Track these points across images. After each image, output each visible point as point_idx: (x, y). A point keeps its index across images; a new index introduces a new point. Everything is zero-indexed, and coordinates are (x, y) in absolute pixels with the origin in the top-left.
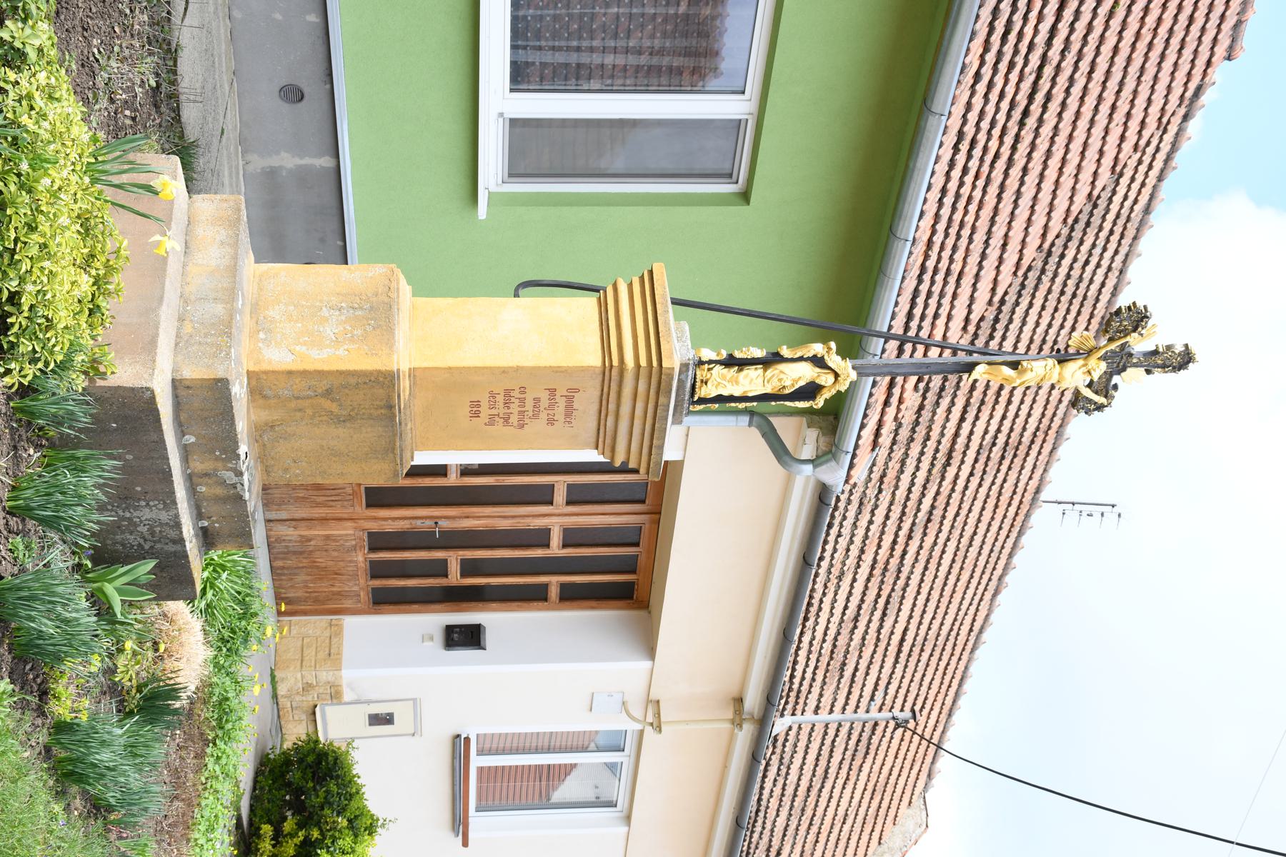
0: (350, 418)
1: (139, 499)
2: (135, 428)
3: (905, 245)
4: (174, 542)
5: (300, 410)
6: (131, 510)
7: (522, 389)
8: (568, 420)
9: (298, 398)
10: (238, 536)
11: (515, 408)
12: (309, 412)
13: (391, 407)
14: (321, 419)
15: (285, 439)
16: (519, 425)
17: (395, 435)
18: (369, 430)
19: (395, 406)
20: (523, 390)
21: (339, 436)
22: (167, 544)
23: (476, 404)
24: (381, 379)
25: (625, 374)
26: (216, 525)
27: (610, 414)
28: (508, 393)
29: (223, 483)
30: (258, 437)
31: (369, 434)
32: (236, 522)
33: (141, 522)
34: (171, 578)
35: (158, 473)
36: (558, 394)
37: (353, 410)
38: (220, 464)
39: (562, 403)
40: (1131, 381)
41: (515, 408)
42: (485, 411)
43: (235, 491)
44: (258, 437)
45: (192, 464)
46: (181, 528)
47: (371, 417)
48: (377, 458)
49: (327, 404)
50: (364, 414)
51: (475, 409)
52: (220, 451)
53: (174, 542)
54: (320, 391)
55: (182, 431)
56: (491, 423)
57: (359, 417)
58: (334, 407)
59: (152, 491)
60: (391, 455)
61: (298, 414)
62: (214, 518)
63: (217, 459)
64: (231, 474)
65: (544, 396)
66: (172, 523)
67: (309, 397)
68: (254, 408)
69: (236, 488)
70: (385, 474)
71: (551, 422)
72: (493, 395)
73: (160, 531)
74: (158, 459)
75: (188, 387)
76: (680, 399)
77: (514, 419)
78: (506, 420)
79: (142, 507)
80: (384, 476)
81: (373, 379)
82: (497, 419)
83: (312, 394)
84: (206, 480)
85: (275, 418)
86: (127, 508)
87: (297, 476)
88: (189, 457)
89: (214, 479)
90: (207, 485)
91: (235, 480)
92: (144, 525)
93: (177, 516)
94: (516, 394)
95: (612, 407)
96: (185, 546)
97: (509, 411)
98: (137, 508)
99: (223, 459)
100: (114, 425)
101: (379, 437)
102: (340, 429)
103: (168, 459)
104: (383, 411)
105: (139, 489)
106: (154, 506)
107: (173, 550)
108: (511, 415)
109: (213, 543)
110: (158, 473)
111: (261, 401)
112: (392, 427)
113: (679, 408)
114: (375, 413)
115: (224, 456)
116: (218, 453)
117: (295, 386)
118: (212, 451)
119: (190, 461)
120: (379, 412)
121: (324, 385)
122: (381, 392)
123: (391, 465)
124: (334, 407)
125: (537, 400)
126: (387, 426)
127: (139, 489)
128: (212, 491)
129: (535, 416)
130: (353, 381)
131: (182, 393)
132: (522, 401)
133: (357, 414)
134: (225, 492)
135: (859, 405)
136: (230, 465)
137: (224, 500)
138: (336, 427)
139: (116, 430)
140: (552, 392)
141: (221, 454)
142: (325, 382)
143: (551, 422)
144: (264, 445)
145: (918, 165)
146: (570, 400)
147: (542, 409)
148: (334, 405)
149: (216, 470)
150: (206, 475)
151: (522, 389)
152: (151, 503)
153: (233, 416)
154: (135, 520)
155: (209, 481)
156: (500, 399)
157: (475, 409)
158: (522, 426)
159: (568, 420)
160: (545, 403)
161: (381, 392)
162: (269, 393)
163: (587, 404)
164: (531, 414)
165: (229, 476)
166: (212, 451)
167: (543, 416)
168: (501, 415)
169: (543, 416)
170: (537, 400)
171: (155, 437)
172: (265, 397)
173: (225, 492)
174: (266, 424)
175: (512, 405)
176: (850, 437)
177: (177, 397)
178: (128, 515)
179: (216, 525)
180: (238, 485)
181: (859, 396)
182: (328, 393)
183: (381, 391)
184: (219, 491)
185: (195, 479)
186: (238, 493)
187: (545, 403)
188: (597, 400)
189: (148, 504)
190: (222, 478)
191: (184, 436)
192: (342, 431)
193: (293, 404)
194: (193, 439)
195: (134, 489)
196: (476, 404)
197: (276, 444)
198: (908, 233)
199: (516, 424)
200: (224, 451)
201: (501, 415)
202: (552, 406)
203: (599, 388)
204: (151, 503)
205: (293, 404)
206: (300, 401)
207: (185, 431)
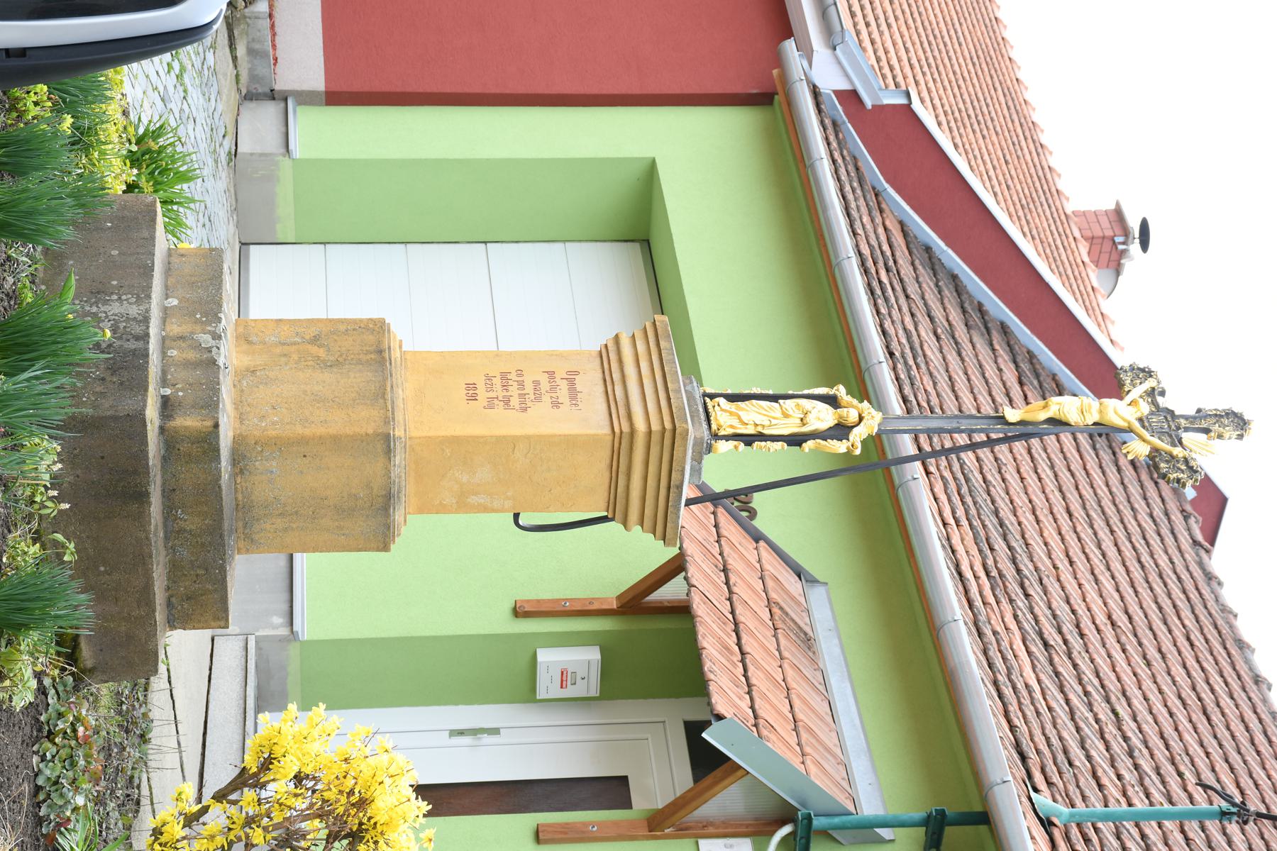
0: (337, 364)
1: (112, 293)
2: (129, 226)
3: (850, 264)
4: (137, 338)
5: (285, 355)
6: (100, 305)
7: (519, 372)
8: (574, 402)
9: (284, 344)
10: (202, 407)
11: (514, 390)
12: (295, 357)
13: (380, 352)
14: (306, 363)
15: (266, 384)
16: (521, 408)
17: (385, 380)
18: (357, 375)
19: (385, 351)
20: (520, 373)
21: (325, 382)
22: (128, 340)
23: (471, 387)
24: (371, 326)
25: (636, 437)
26: (180, 394)
27: (616, 383)
28: (504, 376)
29: (198, 346)
30: (236, 383)
31: (358, 379)
32: (203, 390)
33: (107, 317)
34: (122, 384)
35: (140, 268)
36: (558, 376)
37: (341, 356)
38: (198, 328)
39: (564, 385)
40: (1181, 402)
41: (514, 390)
42: (482, 394)
43: (209, 355)
44: (236, 383)
45: (168, 329)
46: (149, 323)
47: (360, 362)
48: (365, 404)
49: (314, 349)
50: (352, 359)
51: (471, 392)
52: (201, 314)
53: (137, 338)
54: (307, 337)
55: (167, 294)
56: (490, 406)
57: (347, 362)
58: (322, 353)
59: (129, 286)
60: (381, 401)
61: (283, 359)
62: (179, 386)
63: (197, 322)
64: (208, 337)
65: (544, 379)
66: (141, 318)
67: (295, 344)
68: (237, 352)
69: (211, 352)
70: (375, 421)
71: (556, 404)
72: (489, 378)
73: (125, 327)
74: (143, 254)
75: (182, 255)
76: (693, 409)
77: (515, 402)
78: (507, 402)
79: (112, 300)
80: (373, 424)
81: (362, 325)
82: (496, 401)
83: (299, 340)
84: (180, 343)
85: (258, 363)
86: (96, 303)
87: (274, 423)
88: (168, 320)
89: (189, 342)
90: (179, 348)
91: (212, 343)
92: (109, 321)
93: (148, 311)
94: (513, 376)
95: (616, 376)
96: (148, 343)
97: (508, 394)
98: (106, 302)
99: (203, 322)
100: (109, 224)
101: (368, 382)
102: (326, 374)
103: (154, 255)
104: (373, 356)
105: (115, 283)
106: (126, 300)
107: (134, 347)
108: (511, 398)
109: (171, 416)
110: (140, 268)
111: (245, 347)
112: (382, 372)
113: (696, 418)
114: (364, 358)
115: (204, 319)
116: (198, 316)
117: (282, 333)
118: (193, 314)
119: (167, 324)
120: (368, 357)
121: (312, 332)
122: (370, 338)
123: (382, 411)
124: (322, 353)
125: (536, 383)
126: (376, 371)
127: (115, 283)
128: (184, 356)
129: (538, 398)
130: (342, 328)
131: (174, 260)
132: (521, 385)
133: (345, 360)
134: (198, 356)
135: (829, 191)
136: (209, 328)
137: (195, 365)
138: (322, 372)
139: (109, 228)
140: (551, 374)
141: (202, 317)
142: (313, 329)
143: (556, 404)
144: (242, 391)
145: (957, 661)
146: (572, 383)
147: (543, 392)
148: (322, 350)
149: (192, 333)
150: (182, 338)
151: (519, 372)
152: (124, 297)
153: (222, 281)
154: (100, 315)
155: (183, 345)
156: (497, 381)
157: (471, 392)
158: (525, 410)
159: (574, 402)
160: (545, 386)
161: (370, 338)
162: (254, 339)
163: (590, 383)
164: (532, 397)
165: (206, 340)
166: (193, 314)
167: (546, 399)
168: (501, 398)
169: (546, 399)
170: (536, 383)
171: (146, 234)
172: (249, 342)
173: (198, 356)
174: (247, 370)
175: (510, 388)
176: (870, 331)
177: (169, 263)
178: (94, 309)
179: (180, 394)
180: (214, 350)
181: (821, 174)
182: (315, 340)
183: (371, 337)
184: (191, 355)
185: (167, 342)
186: (212, 357)
187: (545, 386)
188: (601, 382)
189: (120, 298)
190: (197, 341)
191: (167, 299)
192: (328, 376)
193: (278, 350)
194: (175, 302)
195: (109, 283)
196: (471, 387)
197: (256, 389)
198: (820, 154)
199: (517, 407)
200: (205, 314)
201: (501, 398)
202: (553, 389)
203: (600, 371)
204: (124, 297)
205: (278, 350)
206: (285, 347)
207: (170, 294)
